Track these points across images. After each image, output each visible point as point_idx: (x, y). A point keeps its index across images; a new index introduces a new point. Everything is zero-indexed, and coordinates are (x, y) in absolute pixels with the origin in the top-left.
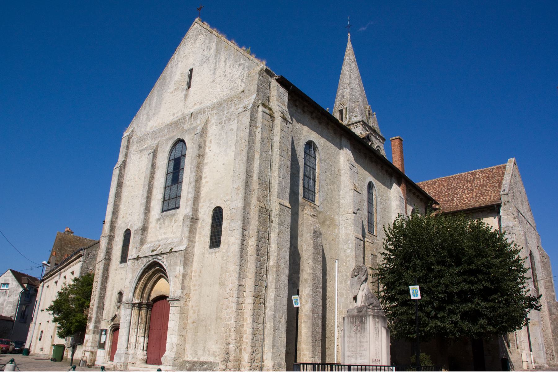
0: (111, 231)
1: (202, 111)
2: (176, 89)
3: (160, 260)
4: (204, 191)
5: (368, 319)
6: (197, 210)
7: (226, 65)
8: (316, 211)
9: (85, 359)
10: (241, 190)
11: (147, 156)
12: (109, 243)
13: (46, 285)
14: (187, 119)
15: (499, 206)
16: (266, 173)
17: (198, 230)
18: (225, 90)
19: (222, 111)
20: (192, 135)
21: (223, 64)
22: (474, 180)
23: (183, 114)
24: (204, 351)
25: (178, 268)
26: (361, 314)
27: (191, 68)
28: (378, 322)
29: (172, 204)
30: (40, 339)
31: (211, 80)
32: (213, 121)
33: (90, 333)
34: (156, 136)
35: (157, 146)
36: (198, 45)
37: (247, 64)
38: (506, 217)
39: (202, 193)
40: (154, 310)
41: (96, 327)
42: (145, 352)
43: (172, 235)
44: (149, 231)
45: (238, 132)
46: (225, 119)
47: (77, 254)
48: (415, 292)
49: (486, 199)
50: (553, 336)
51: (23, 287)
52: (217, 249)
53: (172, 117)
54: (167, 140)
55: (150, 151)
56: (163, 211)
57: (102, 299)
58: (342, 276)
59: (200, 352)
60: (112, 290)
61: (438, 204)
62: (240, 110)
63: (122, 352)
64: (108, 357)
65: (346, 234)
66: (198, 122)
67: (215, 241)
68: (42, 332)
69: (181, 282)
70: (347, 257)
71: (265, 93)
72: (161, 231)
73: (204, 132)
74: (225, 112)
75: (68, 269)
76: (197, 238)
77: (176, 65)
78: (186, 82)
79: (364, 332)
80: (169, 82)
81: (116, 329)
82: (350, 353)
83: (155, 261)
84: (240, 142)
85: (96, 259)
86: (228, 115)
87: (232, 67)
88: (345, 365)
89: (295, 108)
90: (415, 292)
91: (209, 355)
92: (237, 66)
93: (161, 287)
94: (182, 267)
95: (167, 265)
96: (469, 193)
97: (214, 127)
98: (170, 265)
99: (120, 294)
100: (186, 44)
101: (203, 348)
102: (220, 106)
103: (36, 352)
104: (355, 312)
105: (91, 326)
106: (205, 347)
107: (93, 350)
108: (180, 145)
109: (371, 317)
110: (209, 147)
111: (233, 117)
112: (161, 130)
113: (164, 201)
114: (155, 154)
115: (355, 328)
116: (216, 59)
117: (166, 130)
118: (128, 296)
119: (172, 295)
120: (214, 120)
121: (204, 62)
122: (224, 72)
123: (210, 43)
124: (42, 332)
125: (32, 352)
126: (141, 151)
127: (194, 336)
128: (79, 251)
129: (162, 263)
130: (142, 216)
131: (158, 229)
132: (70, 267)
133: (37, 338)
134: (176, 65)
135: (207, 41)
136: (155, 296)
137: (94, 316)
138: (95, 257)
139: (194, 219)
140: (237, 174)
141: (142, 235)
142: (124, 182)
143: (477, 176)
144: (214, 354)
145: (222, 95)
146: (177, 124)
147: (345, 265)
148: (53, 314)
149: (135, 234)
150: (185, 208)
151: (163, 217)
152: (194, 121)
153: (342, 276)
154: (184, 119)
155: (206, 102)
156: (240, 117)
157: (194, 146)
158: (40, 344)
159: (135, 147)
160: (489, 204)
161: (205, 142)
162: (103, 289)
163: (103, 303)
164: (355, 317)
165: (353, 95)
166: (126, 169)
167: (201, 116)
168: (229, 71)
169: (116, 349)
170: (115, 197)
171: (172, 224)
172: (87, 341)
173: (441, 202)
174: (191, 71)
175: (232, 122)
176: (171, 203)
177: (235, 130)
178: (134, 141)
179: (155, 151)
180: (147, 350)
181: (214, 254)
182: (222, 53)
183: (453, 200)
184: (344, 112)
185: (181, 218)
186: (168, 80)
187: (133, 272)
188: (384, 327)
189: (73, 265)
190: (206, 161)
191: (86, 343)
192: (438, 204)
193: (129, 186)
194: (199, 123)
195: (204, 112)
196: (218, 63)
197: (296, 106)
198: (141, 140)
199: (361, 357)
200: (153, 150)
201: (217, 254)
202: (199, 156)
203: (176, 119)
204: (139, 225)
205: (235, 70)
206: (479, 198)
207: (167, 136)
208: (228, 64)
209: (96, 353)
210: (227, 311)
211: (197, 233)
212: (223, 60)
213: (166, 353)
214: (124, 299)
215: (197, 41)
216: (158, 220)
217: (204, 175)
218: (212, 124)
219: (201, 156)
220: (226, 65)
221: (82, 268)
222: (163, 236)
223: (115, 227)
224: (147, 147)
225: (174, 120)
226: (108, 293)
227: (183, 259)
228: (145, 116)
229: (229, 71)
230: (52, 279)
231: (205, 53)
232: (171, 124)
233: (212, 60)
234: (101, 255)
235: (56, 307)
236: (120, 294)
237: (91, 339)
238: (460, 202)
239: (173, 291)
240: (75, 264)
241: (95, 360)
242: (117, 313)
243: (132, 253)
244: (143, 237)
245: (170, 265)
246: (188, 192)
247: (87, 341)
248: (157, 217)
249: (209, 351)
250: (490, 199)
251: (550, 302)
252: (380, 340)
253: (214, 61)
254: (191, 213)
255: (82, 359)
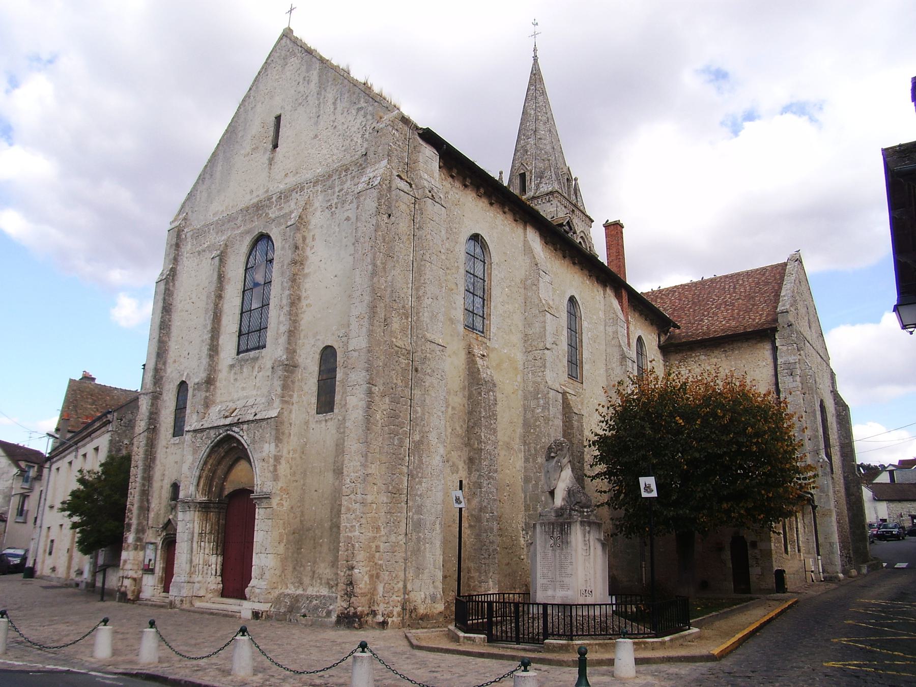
0: (155, 384)
1: (299, 188)
2: (255, 149)
3: (236, 432)
4: (306, 319)
5: (573, 528)
6: (295, 351)
7: (335, 109)
8: (487, 348)
9: (123, 589)
10: (366, 320)
11: (210, 261)
12: (152, 405)
13: (54, 467)
14: (274, 199)
15: (775, 330)
16: (405, 290)
17: (297, 384)
18: (336, 151)
19: (331, 187)
20: (284, 227)
21: (332, 107)
22: (735, 288)
23: (267, 191)
24: (313, 577)
25: (266, 446)
26: (561, 520)
27: (278, 113)
28: (589, 532)
29: (253, 340)
30: (50, 553)
31: (312, 135)
32: (317, 204)
33: (130, 549)
34: (223, 228)
35: (226, 245)
36: (288, 74)
37: (370, 108)
38: (785, 348)
39: (302, 322)
40: (232, 516)
41: (139, 539)
42: (220, 579)
43: (255, 393)
44: (218, 384)
45: (359, 224)
46: (336, 200)
47: (102, 421)
48: (648, 486)
49: (754, 320)
50: (851, 528)
51: (18, 466)
52: (329, 415)
53: (248, 197)
54: (242, 235)
55: (215, 253)
56: (238, 353)
57: (145, 494)
58: (529, 451)
59: (306, 580)
60: (162, 480)
61: (679, 328)
62: (361, 187)
63: (183, 579)
64: (160, 587)
65: (534, 383)
66: (293, 205)
67: (326, 401)
68: (52, 541)
69: (271, 469)
70: (536, 421)
71: (402, 158)
72: (237, 384)
73: (302, 222)
74: (337, 189)
75: (88, 443)
76: (295, 396)
77: (252, 108)
78: (271, 138)
79: (566, 548)
80: (242, 136)
81: (170, 544)
82: (545, 581)
83: (229, 435)
84: (362, 240)
85: (133, 427)
86: (340, 194)
87: (345, 114)
88: (538, 604)
89: (450, 180)
90: (648, 486)
91: (321, 584)
92: (354, 112)
93: (238, 477)
94: (273, 445)
95: (249, 442)
96: (728, 310)
97: (318, 213)
98: (254, 442)
99: (175, 487)
100: (269, 72)
101: (311, 574)
102: (328, 180)
103: (44, 574)
104: (552, 517)
105: (131, 537)
106: (314, 572)
107: (135, 576)
108: (261, 246)
109: (578, 524)
110: (312, 248)
111: (350, 198)
112: (231, 218)
113: (240, 334)
114: (222, 258)
115: (552, 542)
116: (319, 99)
117: (240, 218)
118: (189, 490)
119: (259, 490)
120: (318, 202)
121: (300, 104)
122: (334, 122)
123: (308, 71)
124: (52, 541)
125: (38, 573)
126: (199, 253)
127: (295, 555)
128: (105, 415)
129: (240, 438)
130: (205, 361)
131: (232, 381)
132: (92, 440)
133: (45, 551)
134: (252, 108)
135: (304, 68)
136: (231, 490)
137: (134, 522)
138: (131, 425)
139: (289, 367)
140: (359, 293)
141: (207, 391)
142: (174, 303)
143: (741, 282)
144: (328, 583)
145: (330, 160)
146: (258, 208)
147: (534, 433)
148: (70, 516)
149: (194, 390)
150: (274, 350)
151: (239, 361)
152: (285, 203)
153: (529, 451)
154: (269, 199)
155: (304, 171)
156: (362, 199)
157: (287, 246)
158: (50, 562)
159: (189, 246)
160: (759, 328)
161: (304, 239)
162: (148, 478)
163: (148, 501)
164: (553, 524)
165: (541, 150)
166: (176, 283)
167: (297, 196)
168: (341, 119)
169: (173, 575)
170: (161, 329)
171: (255, 373)
172: (125, 561)
173: (682, 323)
174: (278, 118)
175: (347, 206)
176: (251, 338)
177: (353, 219)
178: (188, 235)
179: (222, 252)
180: (221, 575)
181: (324, 423)
182: (328, 89)
183: (702, 320)
184: (528, 178)
185: (269, 365)
186: (240, 134)
187: (195, 451)
188: (599, 540)
189: (97, 437)
190: (306, 271)
191: (124, 565)
192: (679, 328)
193: (182, 311)
194: (293, 207)
195: (302, 189)
196: (322, 105)
197: (452, 177)
198: (199, 234)
199: (562, 587)
200: (219, 252)
201: (329, 423)
202: (294, 262)
203: (255, 200)
204: (201, 376)
205: (350, 118)
206: (744, 318)
207: (242, 229)
208: (339, 108)
209: (141, 579)
210: (348, 516)
211: (296, 389)
212: (331, 101)
213: (253, 582)
214: (182, 495)
215: (287, 68)
216: (232, 366)
217: (304, 294)
218: (315, 210)
219: (298, 263)
220: (335, 109)
221: (111, 441)
222: (242, 394)
223: (162, 377)
224: (208, 247)
225: (252, 202)
226: (156, 485)
227: (274, 432)
228: (205, 194)
229: (341, 119)
230: (64, 457)
231: (301, 88)
232: (247, 209)
233: (312, 100)
234: (141, 425)
235: (75, 504)
236: (175, 487)
237: (131, 558)
238: (713, 325)
239: (259, 483)
240: (99, 436)
241: (139, 591)
242: (171, 517)
243: (192, 422)
244: (208, 394)
245: (254, 442)
246: (279, 323)
247: (125, 561)
248: (230, 362)
249: (321, 579)
250: (760, 319)
251: (847, 476)
252: (592, 560)
253: (317, 102)
254: (285, 357)
255: (119, 590)
